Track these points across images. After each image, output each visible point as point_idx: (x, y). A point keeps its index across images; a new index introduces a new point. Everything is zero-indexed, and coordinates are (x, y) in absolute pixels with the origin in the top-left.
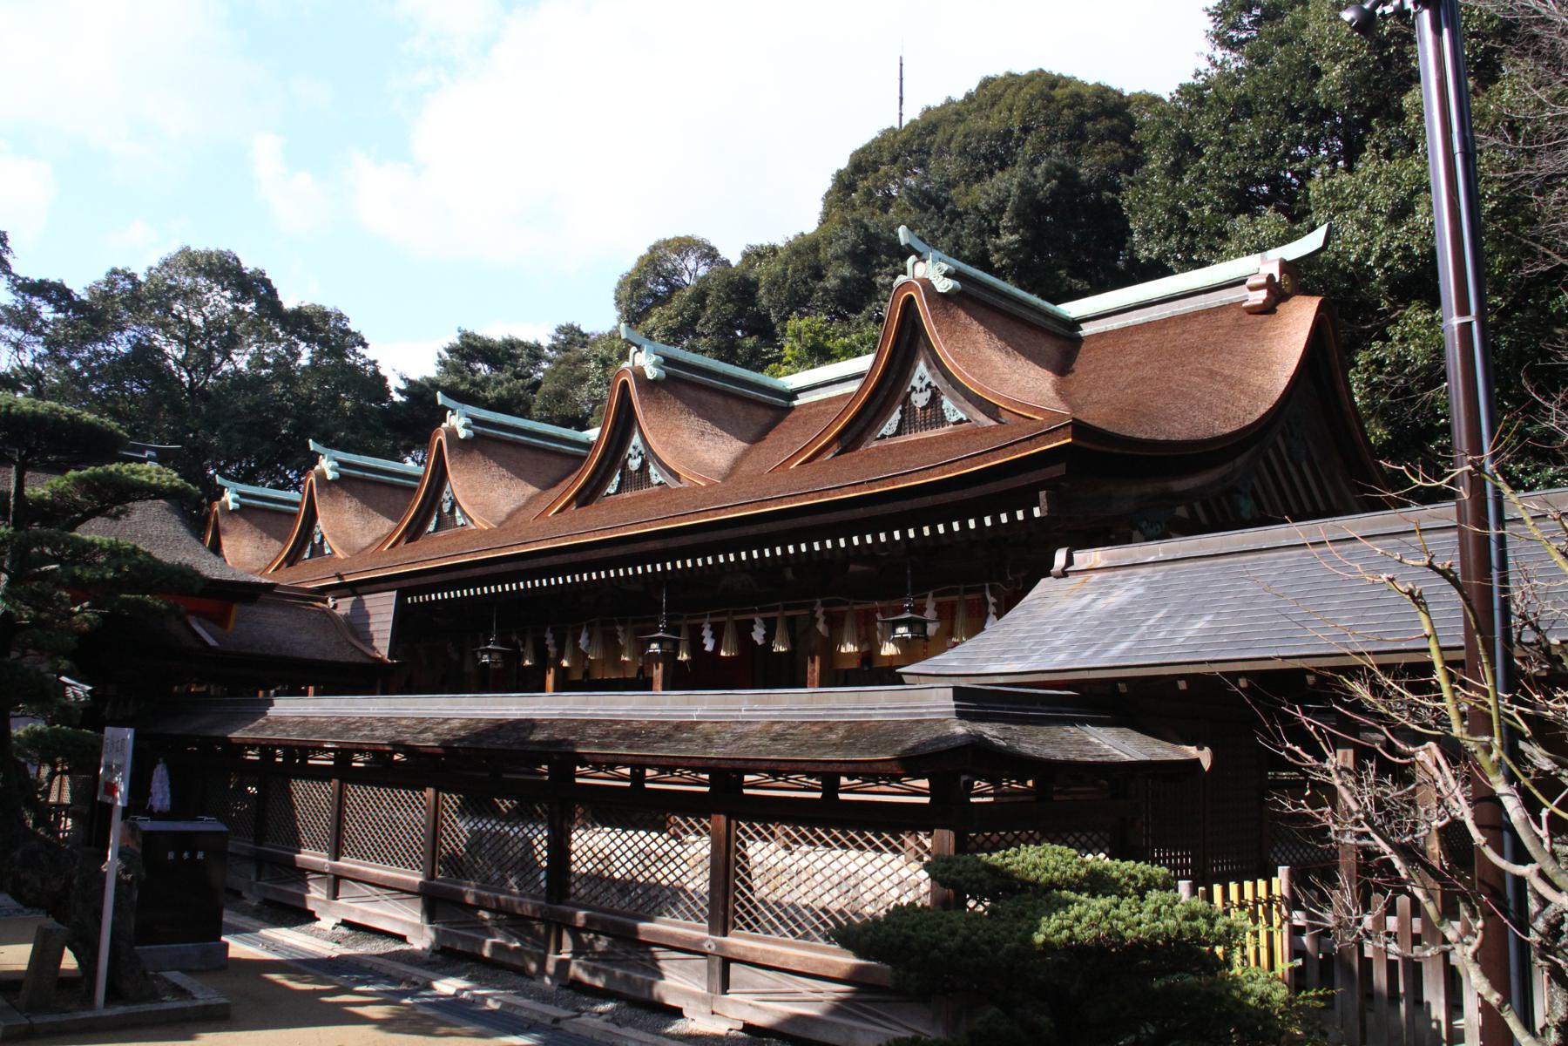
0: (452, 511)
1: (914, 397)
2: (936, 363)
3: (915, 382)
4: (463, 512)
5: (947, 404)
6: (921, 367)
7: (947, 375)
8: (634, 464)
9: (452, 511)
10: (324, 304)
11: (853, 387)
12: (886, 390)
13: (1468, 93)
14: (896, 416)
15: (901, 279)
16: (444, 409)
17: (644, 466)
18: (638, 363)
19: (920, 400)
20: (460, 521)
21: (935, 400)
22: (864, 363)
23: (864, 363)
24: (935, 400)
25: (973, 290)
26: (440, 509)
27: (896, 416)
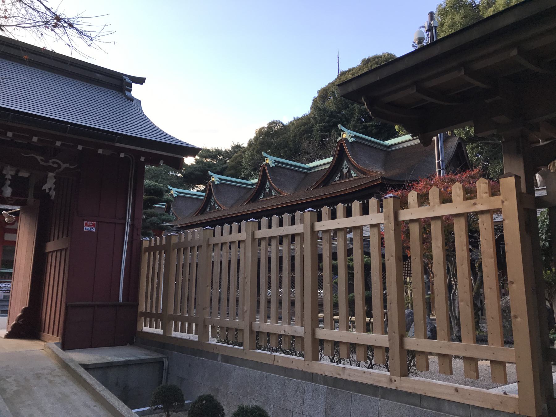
0: (214, 205)
1: (343, 170)
2: (349, 161)
3: (344, 166)
4: (218, 205)
5: (352, 172)
6: (345, 162)
7: (352, 164)
8: (268, 190)
9: (214, 205)
10: (259, 127)
11: (328, 166)
12: (336, 167)
13: (352, 167)
14: (339, 175)
15: (339, 138)
16: (342, 131)
17: (270, 191)
18: (267, 162)
19: (345, 171)
20: (217, 207)
21: (349, 171)
22: (330, 159)
23: (330, 159)
24: (349, 171)
25: (359, 140)
26: (211, 204)
27: (339, 175)
